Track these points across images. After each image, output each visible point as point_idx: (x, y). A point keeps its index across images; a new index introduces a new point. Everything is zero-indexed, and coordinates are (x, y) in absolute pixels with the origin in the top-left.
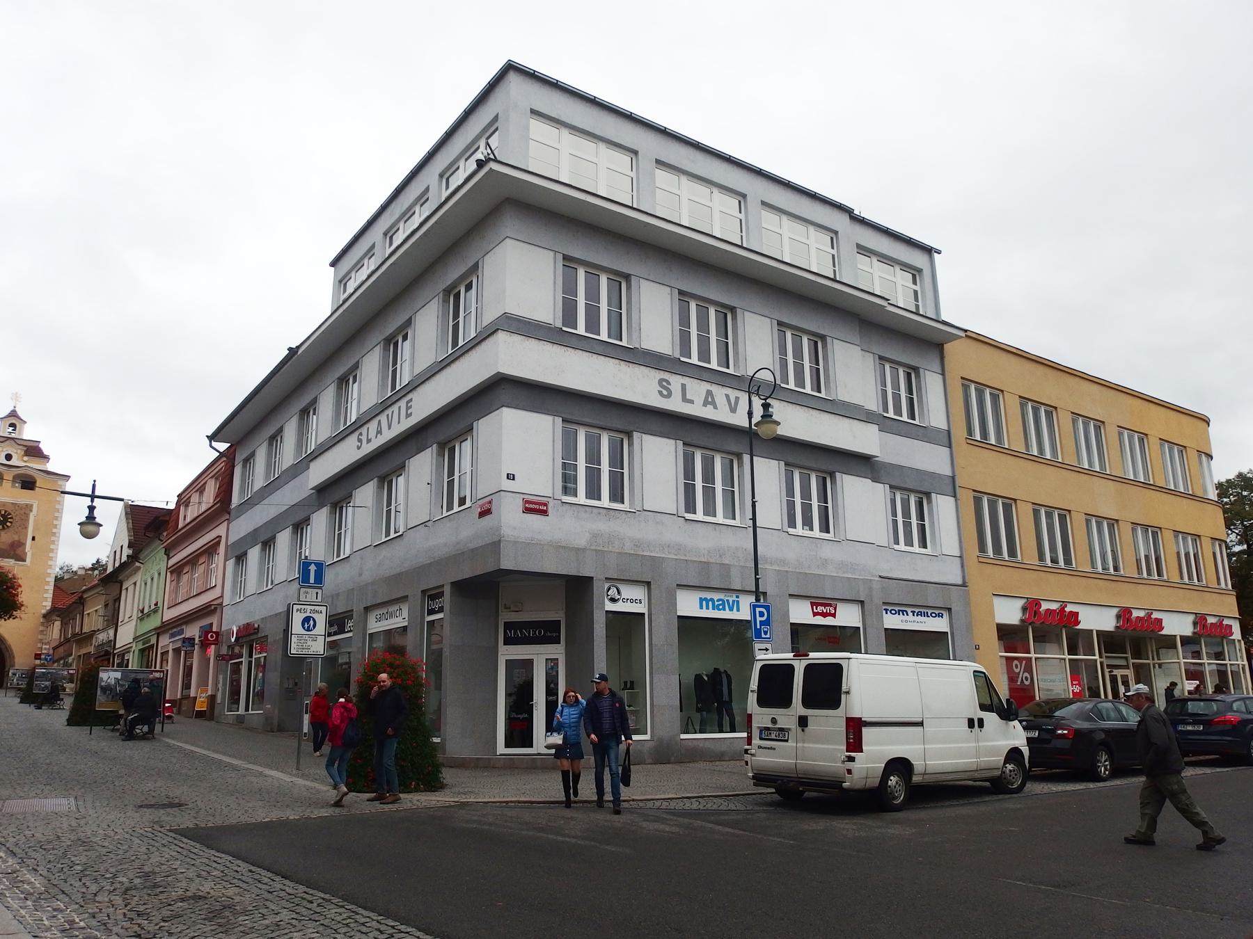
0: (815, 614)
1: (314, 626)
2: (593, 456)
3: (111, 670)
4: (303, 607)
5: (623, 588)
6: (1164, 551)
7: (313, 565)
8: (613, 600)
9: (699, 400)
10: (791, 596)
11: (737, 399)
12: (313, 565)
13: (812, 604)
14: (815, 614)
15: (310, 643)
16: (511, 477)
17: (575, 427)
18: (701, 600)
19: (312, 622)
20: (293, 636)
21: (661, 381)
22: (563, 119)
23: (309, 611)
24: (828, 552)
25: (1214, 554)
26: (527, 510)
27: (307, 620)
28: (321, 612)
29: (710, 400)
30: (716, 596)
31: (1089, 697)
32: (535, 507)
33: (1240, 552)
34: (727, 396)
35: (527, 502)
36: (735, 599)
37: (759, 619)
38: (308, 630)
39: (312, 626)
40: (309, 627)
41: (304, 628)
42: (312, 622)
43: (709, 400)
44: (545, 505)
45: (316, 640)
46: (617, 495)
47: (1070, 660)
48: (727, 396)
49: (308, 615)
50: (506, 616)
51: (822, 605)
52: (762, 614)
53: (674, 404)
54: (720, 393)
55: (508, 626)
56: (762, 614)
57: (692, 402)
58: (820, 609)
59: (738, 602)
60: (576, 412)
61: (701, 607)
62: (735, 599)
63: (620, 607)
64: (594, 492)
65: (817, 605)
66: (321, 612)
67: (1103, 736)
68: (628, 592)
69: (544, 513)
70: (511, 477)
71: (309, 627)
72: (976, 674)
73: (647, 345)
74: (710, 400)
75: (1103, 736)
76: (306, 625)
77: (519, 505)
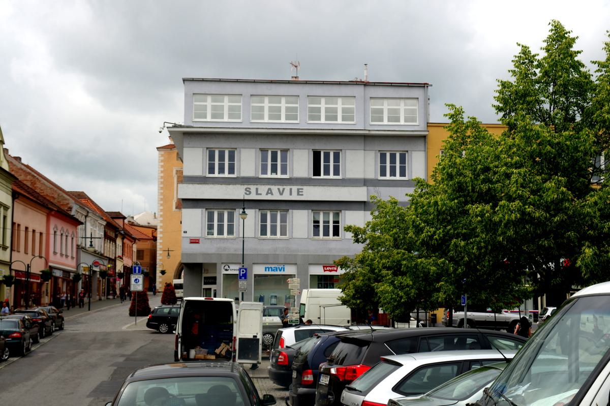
0: (325, 271)
2: (221, 219)
3: (540, 326)
5: (230, 266)
8: (226, 270)
9: (264, 193)
10: (253, 263)
11: (284, 189)
13: (324, 267)
14: (325, 271)
16: (185, 232)
17: (212, 210)
18: (266, 268)
21: (246, 189)
22: (207, 93)
24: (333, 245)
25: (101, 246)
26: (191, 243)
27: (136, 280)
29: (270, 192)
30: (273, 266)
32: (195, 241)
34: (279, 189)
35: (191, 240)
36: (282, 266)
37: (241, 273)
38: (137, 283)
43: (270, 192)
44: (198, 240)
46: (283, 233)
48: (279, 189)
50: (204, 275)
51: (329, 267)
52: (243, 271)
53: (253, 196)
54: (275, 189)
55: (205, 278)
56: (243, 271)
57: (261, 194)
58: (328, 268)
59: (284, 268)
60: (211, 205)
61: (266, 270)
62: (282, 266)
63: (229, 272)
64: (220, 232)
65: (327, 267)
68: (232, 267)
69: (198, 243)
70: (185, 232)
73: (350, 175)
74: (270, 192)
77: (189, 241)
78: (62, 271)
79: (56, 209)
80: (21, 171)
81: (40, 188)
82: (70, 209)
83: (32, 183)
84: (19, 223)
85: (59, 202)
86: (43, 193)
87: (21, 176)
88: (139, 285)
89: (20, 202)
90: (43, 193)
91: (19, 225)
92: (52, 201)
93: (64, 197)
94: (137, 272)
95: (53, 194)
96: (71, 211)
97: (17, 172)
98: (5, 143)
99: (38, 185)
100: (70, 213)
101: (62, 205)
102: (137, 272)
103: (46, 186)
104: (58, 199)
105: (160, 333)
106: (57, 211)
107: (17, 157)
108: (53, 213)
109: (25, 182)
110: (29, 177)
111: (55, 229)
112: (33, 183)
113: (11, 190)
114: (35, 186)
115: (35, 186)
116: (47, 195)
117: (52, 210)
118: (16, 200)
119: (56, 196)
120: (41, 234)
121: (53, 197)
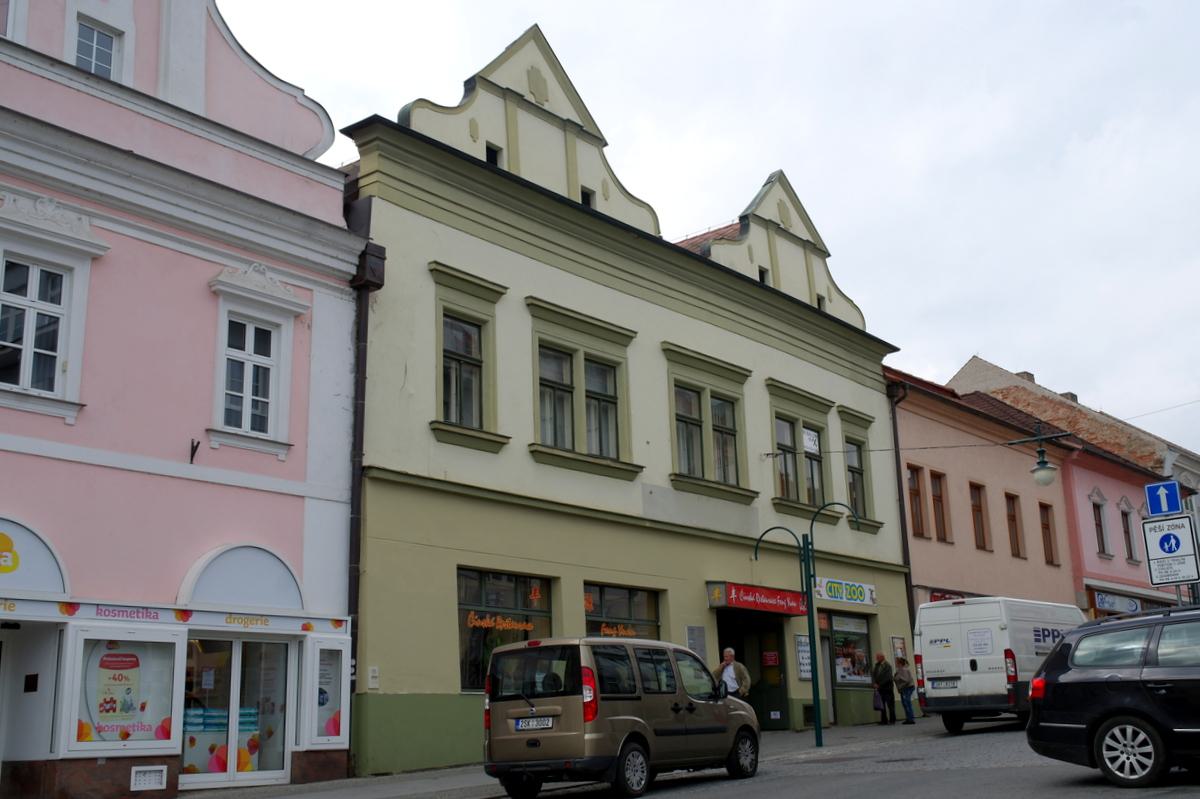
1: (1178, 545)
4: (1157, 524)
6: (736, 493)
7: (1162, 488)
12: (1162, 488)
15: (1176, 567)
19: (1173, 541)
20: (1193, 553)
23: (1166, 528)
27: (1165, 539)
28: (1183, 526)
31: (1169, 510)
33: (658, 681)
38: (1170, 551)
39: (1174, 545)
40: (1170, 548)
41: (1164, 550)
42: (1173, 541)
45: (1184, 563)
47: (20, 314)
49: (1166, 532)
66: (1183, 526)
67: (104, 762)
71: (1170, 548)
72: (462, 572)
75: (104, 762)
76: (1166, 547)
78: (1138, 602)
79: (1080, 447)
80: (1044, 403)
81: (1088, 431)
82: (1160, 462)
83: (1070, 422)
84: (939, 469)
85: (1131, 452)
86: (1096, 438)
87: (1045, 412)
88: (1182, 559)
89: (910, 408)
90: (1096, 438)
91: (937, 477)
92: (1116, 453)
93: (1141, 440)
94: (1164, 506)
95: (1117, 437)
96: (1162, 467)
97: (1037, 406)
98: (608, 141)
99: (1083, 424)
100: (1160, 473)
101: (1141, 458)
102: (1164, 506)
103: (1100, 423)
104: (1131, 446)
105: (1107, 781)
106: (1086, 452)
107: (1066, 394)
108: (1075, 455)
109: (1055, 424)
110: (1062, 412)
111: (1124, 507)
112: (1072, 422)
113: (881, 379)
114: (1077, 427)
115: (1077, 427)
116: (1105, 442)
117: (1072, 449)
118: (900, 404)
119: (1124, 441)
120: (1045, 508)
121: (1118, 444)
